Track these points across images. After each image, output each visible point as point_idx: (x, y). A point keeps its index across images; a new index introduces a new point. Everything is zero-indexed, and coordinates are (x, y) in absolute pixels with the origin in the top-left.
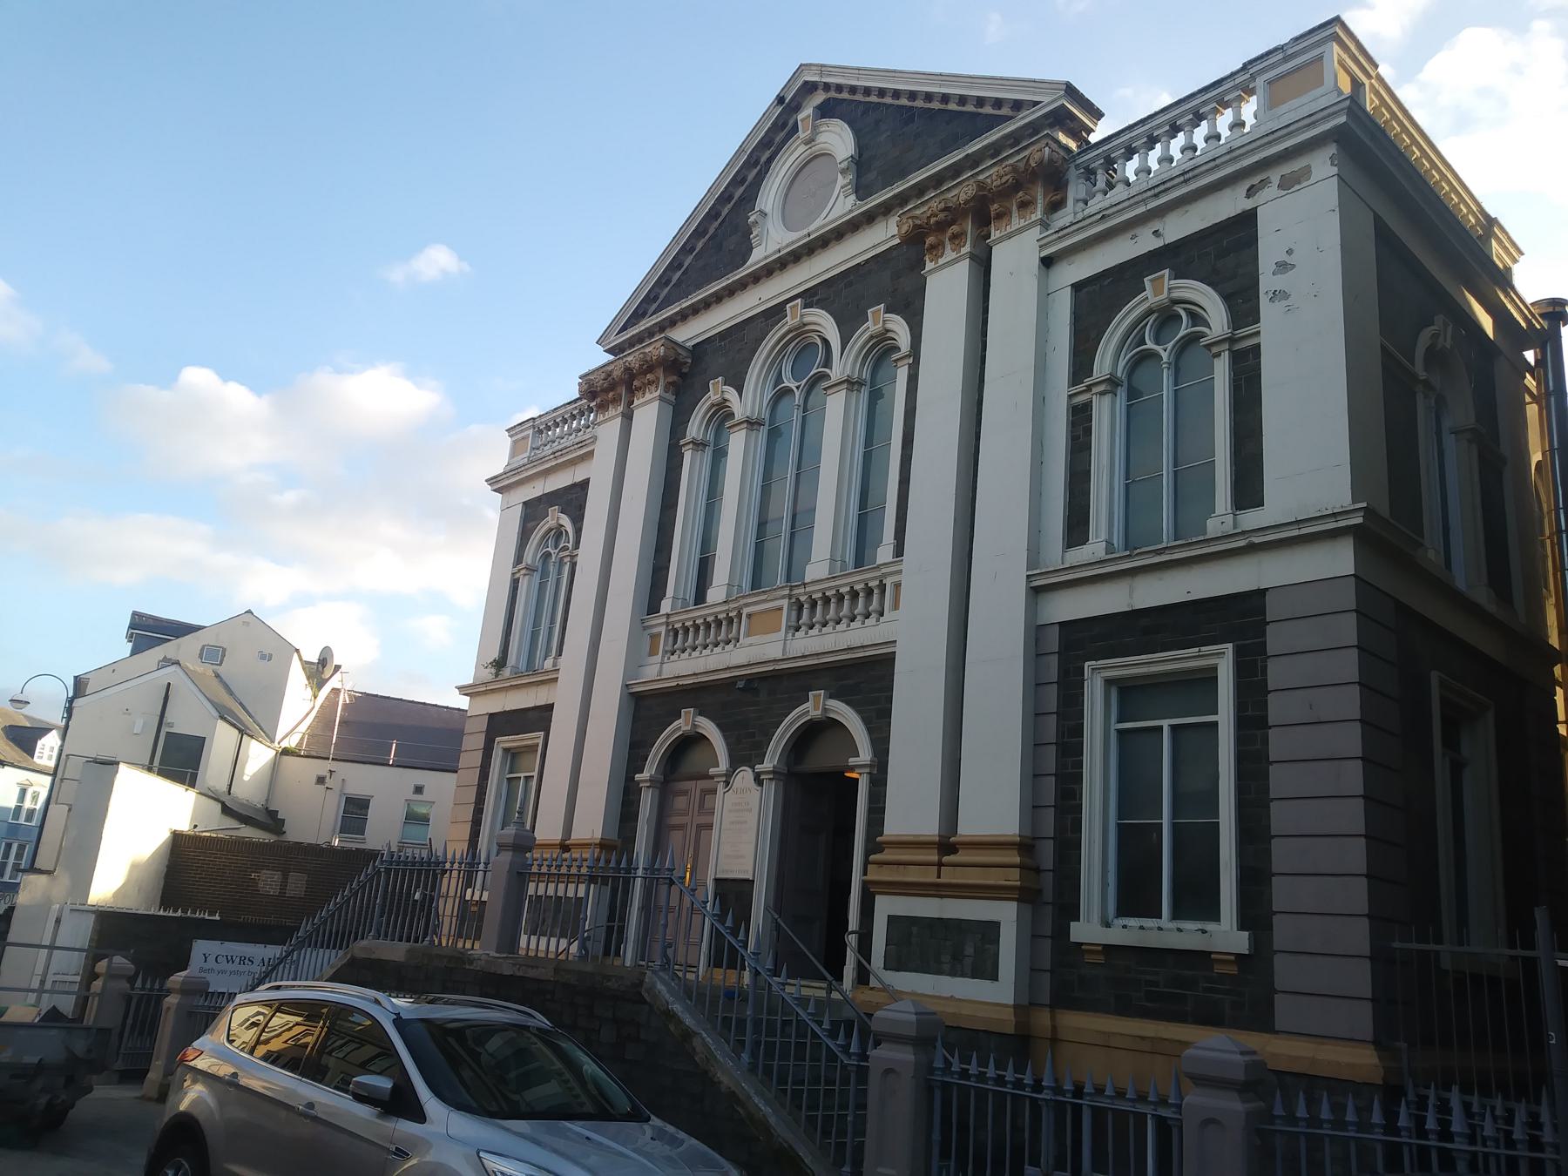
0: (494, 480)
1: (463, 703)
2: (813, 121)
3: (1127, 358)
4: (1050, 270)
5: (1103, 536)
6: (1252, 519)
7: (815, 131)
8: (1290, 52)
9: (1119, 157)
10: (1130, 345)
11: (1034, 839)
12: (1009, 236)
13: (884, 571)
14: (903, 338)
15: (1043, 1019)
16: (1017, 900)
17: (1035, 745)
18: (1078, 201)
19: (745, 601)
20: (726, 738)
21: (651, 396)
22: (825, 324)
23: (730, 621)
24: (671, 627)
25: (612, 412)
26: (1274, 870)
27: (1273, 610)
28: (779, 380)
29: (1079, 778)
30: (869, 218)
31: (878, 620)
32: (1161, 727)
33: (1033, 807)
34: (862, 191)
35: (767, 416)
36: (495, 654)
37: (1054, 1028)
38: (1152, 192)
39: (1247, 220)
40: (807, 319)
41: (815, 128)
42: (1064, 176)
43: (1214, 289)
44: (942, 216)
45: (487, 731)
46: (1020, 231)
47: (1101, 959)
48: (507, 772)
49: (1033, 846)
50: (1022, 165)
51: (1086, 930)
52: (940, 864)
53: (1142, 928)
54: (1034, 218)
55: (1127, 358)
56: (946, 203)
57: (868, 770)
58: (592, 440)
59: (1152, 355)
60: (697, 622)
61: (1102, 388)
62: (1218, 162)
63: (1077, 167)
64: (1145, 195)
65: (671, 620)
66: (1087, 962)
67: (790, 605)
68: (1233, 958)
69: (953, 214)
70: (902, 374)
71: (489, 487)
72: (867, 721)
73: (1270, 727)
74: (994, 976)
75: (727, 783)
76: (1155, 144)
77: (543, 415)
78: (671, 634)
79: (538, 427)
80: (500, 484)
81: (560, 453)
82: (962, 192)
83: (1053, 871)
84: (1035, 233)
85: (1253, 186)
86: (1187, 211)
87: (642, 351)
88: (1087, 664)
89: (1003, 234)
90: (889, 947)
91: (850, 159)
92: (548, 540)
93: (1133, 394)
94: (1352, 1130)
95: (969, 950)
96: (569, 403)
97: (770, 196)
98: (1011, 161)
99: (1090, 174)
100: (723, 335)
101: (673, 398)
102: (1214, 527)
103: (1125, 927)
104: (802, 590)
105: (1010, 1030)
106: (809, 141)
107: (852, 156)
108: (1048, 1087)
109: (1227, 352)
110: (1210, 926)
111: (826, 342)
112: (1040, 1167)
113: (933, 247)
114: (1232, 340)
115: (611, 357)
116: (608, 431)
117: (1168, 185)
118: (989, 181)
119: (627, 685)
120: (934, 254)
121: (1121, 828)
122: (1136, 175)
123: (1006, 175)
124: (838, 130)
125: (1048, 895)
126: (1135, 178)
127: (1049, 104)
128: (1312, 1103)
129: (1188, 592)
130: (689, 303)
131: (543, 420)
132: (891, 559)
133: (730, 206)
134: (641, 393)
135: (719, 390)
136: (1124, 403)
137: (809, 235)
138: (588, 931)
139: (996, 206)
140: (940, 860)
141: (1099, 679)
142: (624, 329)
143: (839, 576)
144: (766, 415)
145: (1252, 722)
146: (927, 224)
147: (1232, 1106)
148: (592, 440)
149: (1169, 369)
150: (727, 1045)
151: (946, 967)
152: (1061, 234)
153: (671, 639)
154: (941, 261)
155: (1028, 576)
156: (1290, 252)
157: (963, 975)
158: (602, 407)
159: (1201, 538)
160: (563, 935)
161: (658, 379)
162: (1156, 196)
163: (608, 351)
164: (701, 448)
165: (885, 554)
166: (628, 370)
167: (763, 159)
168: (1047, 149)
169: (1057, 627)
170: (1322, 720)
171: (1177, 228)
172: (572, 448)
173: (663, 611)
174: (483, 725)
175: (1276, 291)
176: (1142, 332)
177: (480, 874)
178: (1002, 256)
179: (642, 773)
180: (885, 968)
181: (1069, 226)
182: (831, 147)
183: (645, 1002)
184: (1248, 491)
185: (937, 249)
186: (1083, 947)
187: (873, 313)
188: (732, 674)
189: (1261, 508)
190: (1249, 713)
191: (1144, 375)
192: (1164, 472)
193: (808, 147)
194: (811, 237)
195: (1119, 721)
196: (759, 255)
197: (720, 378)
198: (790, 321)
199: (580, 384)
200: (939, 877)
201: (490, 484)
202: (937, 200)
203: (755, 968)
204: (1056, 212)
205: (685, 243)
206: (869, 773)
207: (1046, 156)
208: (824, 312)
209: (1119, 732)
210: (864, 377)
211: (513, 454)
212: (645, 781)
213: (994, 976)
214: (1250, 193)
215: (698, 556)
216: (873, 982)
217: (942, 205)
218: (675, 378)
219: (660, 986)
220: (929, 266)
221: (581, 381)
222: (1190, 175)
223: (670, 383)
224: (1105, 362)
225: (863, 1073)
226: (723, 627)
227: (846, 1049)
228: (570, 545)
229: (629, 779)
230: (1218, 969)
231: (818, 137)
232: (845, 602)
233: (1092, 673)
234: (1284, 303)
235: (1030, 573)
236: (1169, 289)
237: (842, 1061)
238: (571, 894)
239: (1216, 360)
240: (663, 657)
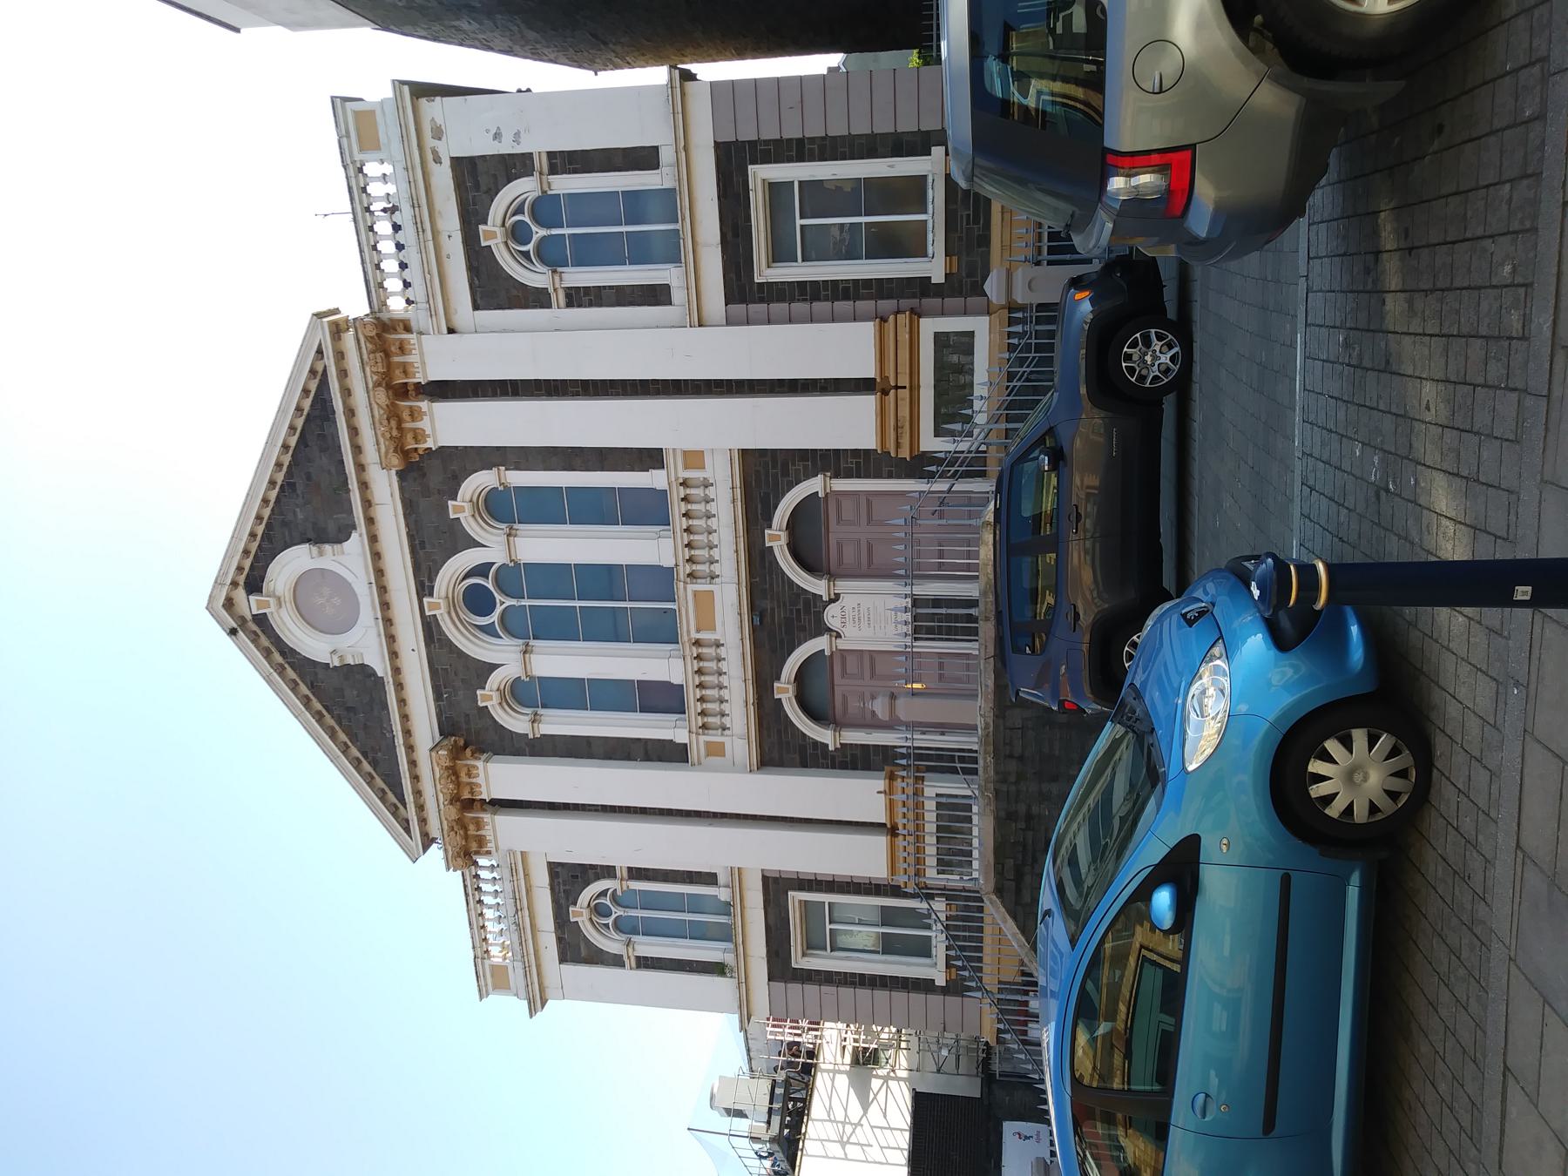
7: (272, 595)
8: (344, 132)
24: (701, 730)
32: (802, 226)
38: (421, 233)
40: (443, 594)
47: (955, 259)
58: (512, 855)
64: (422, 240)
65: (694, 730)
71: (538, 1014)
74: (971, 334)
75: (838, 636)
80: (537, 1001)
86: (440, 212)
97: (316, 647)
117: (418, 221)
119: (751, 771)
127: (324, 334)
135: (489, 696)
142: (407, 830)
145: (799, 150)
148: (512, 855)
156: (488, 131)
161: (467, 765)
162: (423, 231)
170: (800, 100)
173: (686, 741)
182: (288, 587)
184: (644, 158)
194: (373, 581)
198: (441, 613)
200: (905, 387)
206: (831, 478)
209: (803, 261)
213: (971, 334)
214: (438, 160)
217: (385, 423)
222: (415, 202)
224: (536, 277)
226: (703, 655)
231: (277, 594)
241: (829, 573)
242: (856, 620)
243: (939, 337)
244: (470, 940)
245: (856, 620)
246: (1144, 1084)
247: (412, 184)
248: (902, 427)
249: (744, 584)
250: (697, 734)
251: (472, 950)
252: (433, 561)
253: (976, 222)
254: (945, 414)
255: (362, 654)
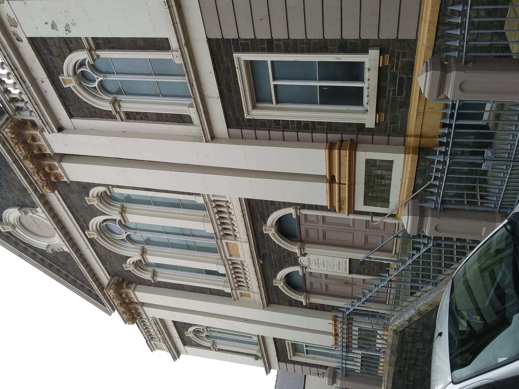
0: (174, 358)
1: (274, 372)
2: (4, 225)
3: (102, 95)
4: (65, 127)
5: (186, 108)
6: (174, 44)
9: (9, 96)
10: (95, 92)
11: (327, 142)
12: (49, 146)
13: (207, 201)
14: (102, 189)
15: (411, 141)
16: (355, 151)
17: (284, 141)
18: (31, 115)
19: (224, 258)
20: (286, 267)
21: (133, 294)
22: (95, 221)
23: (234, 263)
25: (141, 311)
26: (339, 37)
27: (216, 35)
28: (123, 240)
29: (299, 122)
30: (47, 204)
31: (230, 203)
32: (275, 86)
33: (312, 142)
34: (33, 206)
35: (140, 245)
36: (252, 359)
37: (415, 136)
38: (23, 84)
39: (32, 41)
41: (7, 224)
42: (20, 121)
43: (67, 56)
44: (41, 175)
45: (286, 362)
46: (46, 141)
47: (383, 115)
48: (304, 355)
49: (331, 143)
50: (15, 141)
51: (370, 121)
52: (340, 183)
53: (368, 96)
54: (39, 135)
55: (102, 95)
56: (35, 173)
57: (298, 210)
59: (101, 83)
60: (234, 277)
61: (117, 107)
62: (6, 55)
63: (15, 115)
66: (384, 120)
67: (225, 239)
68: (378, 115)
69: (40, 169)
70: (116, 190)
72: (276, 209)
73: (272, 38)
76: (2, 80)
77: (144, 337)
78: (240, 287)
79: (149, 339)
80: (176, 354)
81: (161, 332)
82: (29, 165)
83: (342, 134)
84: (46, 134)
85: (17, 39)
86: (31, 68)
87: (112, 299)
88: (246, 117)
89: (48, 149)
90: (378, 206)
91: (20, 210)
92: (201, 336)
93: (119, 92)
94: (466, 20)
95: (379, 172)
96: (139, 327)
97: (41, 244)
98: (13, 145)
99: (19, 109)
100: (104, 264)
101: (134, 285)
102: (179, 61)
103: (367, 104)
104: (218, 234)
105: (416, 157)
106: (14, 226)
107: (19, 210)
108: (444, 158)
109: (96, 52)
110: (367, 66)
111: (104, 221)
112: (482, 163)
113: (56, 178)
114: (90, 50)
115: (116, 311)
116: (150, 313)
117: (19, 77)
118: (23, 155)
119: (263, 308)
120: (59, 177)
121: (321, 103)
122: (17, 89)
123: (19, 148)
124: (8, 215)
125: (354, 137)
126: (18, 90)
128: (453, 13)
129: (210, 72)
130: (90, 278)
131: (147, 337)
132: (202, 197)
133: (46, 259)
134: (131, 299)
135: (129, 266)
136: (124, 96)
137: (55, 229)
138: (373, 327)
139: (35, 152)
140: (338, 184)
141: (252, 112)
142: (103, 304)
143: (210, 218)
144: (140, 246)
146: (46, 181)
147: (453, 77)
149: (106, 77)
150: (424, 295)
151: (387, 182)
152: (45, 123)
153: (242, 288)
154: (63, 174)
155: (206, 142)
157: (391, 175)
158: (139, 314)
159: (184, 67)
160: (375, 337)
161: (125, 292)
162: (24, 82)
163: (114, 312)
164: (156, 273)
165: (200, 200)
166: (121, 305)
167: (24, 246)
168: (5, 130)
169: (228, 129)
171: (40, 73)
172: (158, 327)
174: (283, 364)
175: (65, 30)
176: (91, 88)
177: (347, 366)
178: (58, 149)
179: (303, 302)
180: (388, 207)
181: (42, 120)
183: (404, 329)
185: (57, 177)
186: (377, 122)
187: (89, 202)
188: (257, 264)
189: (169, 39)
190: (266, 46)
191: (111, 87)
192: (156, 80)
193: (16, 227)
194: (56, 228)
195: (272, 103)
196: (66, 248)
197: (123, 265)
198: (95, 236)
199: (129, 324)
200: (346, 184)
201: (176, 360)
202: (34, 177)
203: (388, 281)
204: (37, 125)
205: (63, 279)
206: (299, 209)
207: (9, 130)
208: (91, 222)
209: (277, 102)
210: (120, 205)
211: (162, 349)
212: (306, 301)
215: (205, 275)
216: (395, 213)
217: (36, 175)
218: (124, 284)
219: (397, 322)
220: (65, 179)
221: (127, 324)
222: (13, 67)
223: (127, 287)
224: (106, 106)
225: (436, 238)
227: (425, 245)
228: (202, 328)
229: (306, 307)
230: (387, 63)
232: (222, 216)
233: (250, 115)
234: (71, 26)
235: (204, 141)
236: (69, 76)
237: (431, 247)
238: (357, 333)
239: (101, 57)
240: (251, 292)
241: (301, 241)
242: (317, 264)
243: (368, 161)
244: (143, 337)
245: (317, 264)
246: (440, 27)
247: (7, 57)
248: (343, 201)
249: (253, 246)
250: (236, 290)
251: (145, 339)
252: (85, 218)
253: (400, 93)
254: (371, 196)
255: (62, 248)
